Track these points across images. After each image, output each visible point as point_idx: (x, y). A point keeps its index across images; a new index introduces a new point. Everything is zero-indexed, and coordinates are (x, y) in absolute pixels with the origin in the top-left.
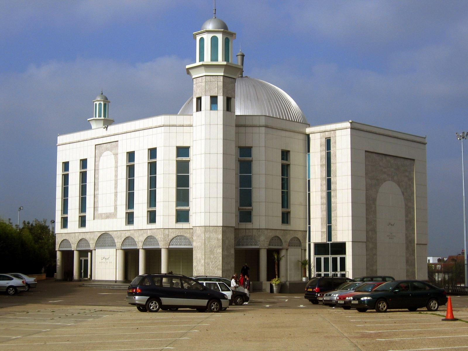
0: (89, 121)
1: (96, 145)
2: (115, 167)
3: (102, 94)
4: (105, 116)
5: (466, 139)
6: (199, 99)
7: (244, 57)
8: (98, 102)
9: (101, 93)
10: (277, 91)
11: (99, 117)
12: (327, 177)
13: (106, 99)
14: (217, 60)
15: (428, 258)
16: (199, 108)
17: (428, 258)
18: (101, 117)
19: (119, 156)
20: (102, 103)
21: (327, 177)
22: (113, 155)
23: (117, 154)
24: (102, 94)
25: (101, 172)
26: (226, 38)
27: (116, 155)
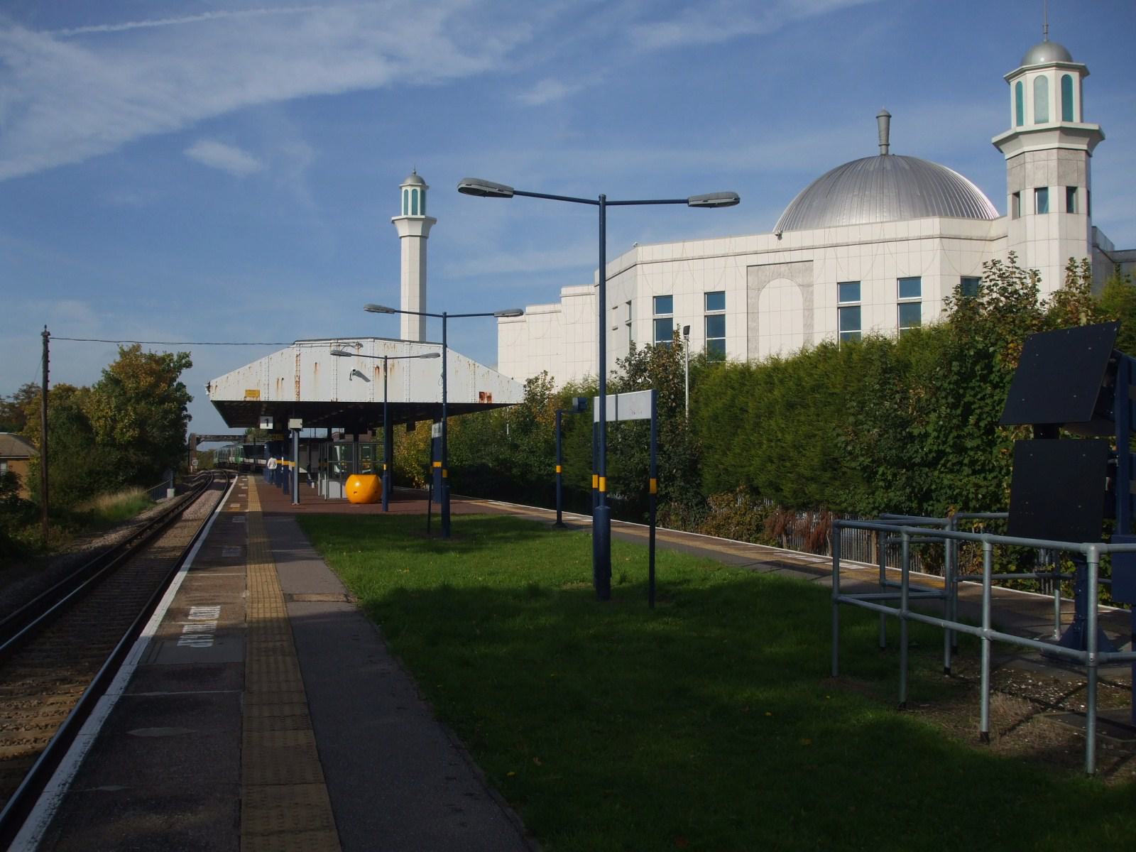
0: (393, 221)
1: (748, 266)
2: (804, 309)
3: (415, 173)
4: (422, 213)
5: (1129, 276)
6: (1042, 192)
7: (891, 119)
8: (408, 188)
9: (414, 172)
10: (964, 184)
11: (413, 214)
12: (841, 330)
13: (423, 182)
14: (1071, 120)
15: (272, 418)
16: (1042, 206)
17: (272, 418)
18: (417, 214)
19: (817, 289)
20: (418, 189)
21: (841, 330)
22: (798, 288)
23: (811, 285)
24: (415, 173)
25: (763, 320)
26: (1063, 77)
27: (807, 287)
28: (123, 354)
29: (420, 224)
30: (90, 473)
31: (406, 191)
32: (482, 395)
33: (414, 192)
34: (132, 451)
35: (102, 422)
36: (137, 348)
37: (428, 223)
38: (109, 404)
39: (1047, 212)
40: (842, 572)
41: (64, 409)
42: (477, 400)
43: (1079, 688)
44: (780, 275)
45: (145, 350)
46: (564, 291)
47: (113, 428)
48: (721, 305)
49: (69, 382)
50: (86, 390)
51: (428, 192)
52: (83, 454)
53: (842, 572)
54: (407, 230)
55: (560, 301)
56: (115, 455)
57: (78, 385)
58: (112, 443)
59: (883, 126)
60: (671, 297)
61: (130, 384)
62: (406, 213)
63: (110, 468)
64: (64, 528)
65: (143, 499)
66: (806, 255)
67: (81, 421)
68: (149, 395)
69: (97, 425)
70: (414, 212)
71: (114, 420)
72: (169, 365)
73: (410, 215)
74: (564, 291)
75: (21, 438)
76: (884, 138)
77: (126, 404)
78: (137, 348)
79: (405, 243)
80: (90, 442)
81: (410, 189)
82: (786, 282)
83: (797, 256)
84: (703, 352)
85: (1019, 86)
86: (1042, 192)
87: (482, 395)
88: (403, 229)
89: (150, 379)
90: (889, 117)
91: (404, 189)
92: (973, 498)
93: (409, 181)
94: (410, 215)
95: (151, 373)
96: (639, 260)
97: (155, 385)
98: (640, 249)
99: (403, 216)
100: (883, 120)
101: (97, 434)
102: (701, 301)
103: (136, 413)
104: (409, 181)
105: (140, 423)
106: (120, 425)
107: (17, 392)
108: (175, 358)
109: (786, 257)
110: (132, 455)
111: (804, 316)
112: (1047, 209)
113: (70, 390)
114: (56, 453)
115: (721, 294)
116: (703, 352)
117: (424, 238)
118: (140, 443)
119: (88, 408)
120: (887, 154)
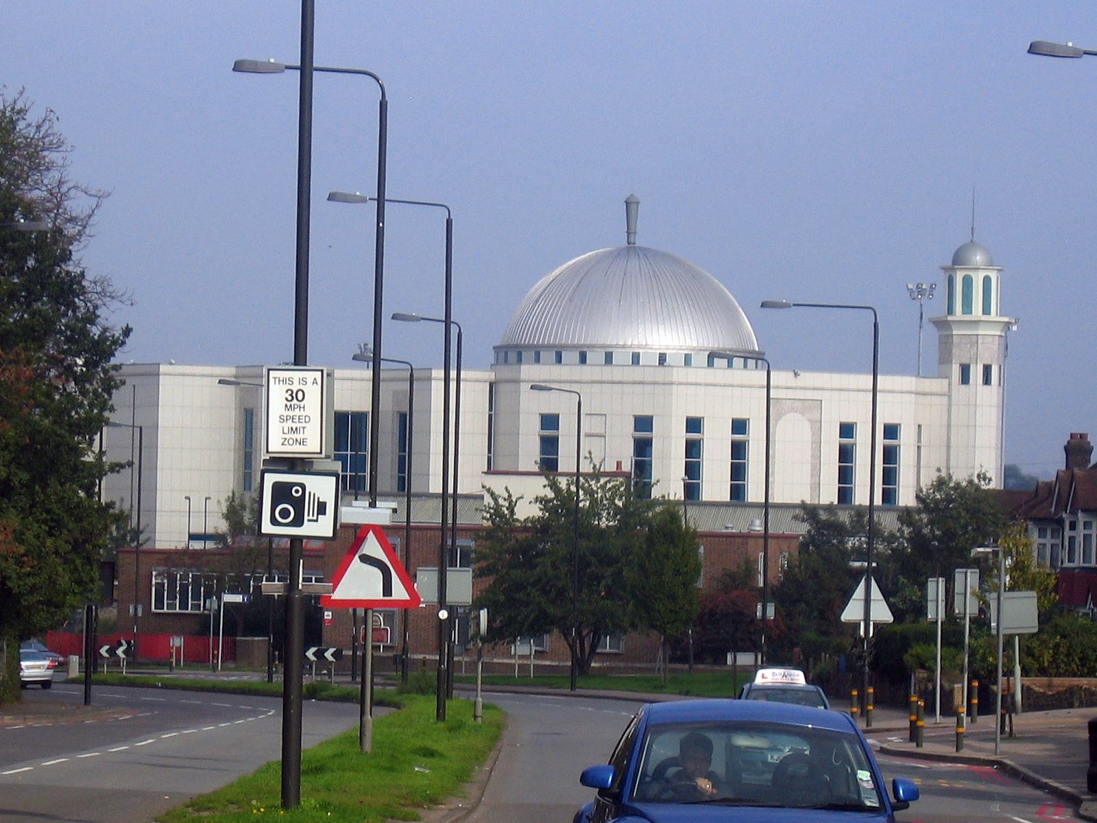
6: (987, 369)
11: (964, 313)
28: (111, 501)
39: (990, 384)
40: (1083, 783)
43: (56, 221)
44: (794, 410)
53: (1083, 783)
60: (733, 421)
66: (816, 395)
82: (798, 416)
83: (809, 395)
84: (71, 267)
86: (987, 369)
92: (1038, 639)
96: (675, 379)
107: (123, 387)
109: (800, 394)
111: (812, 447)
112: (991, 382)
116: (71, 267)
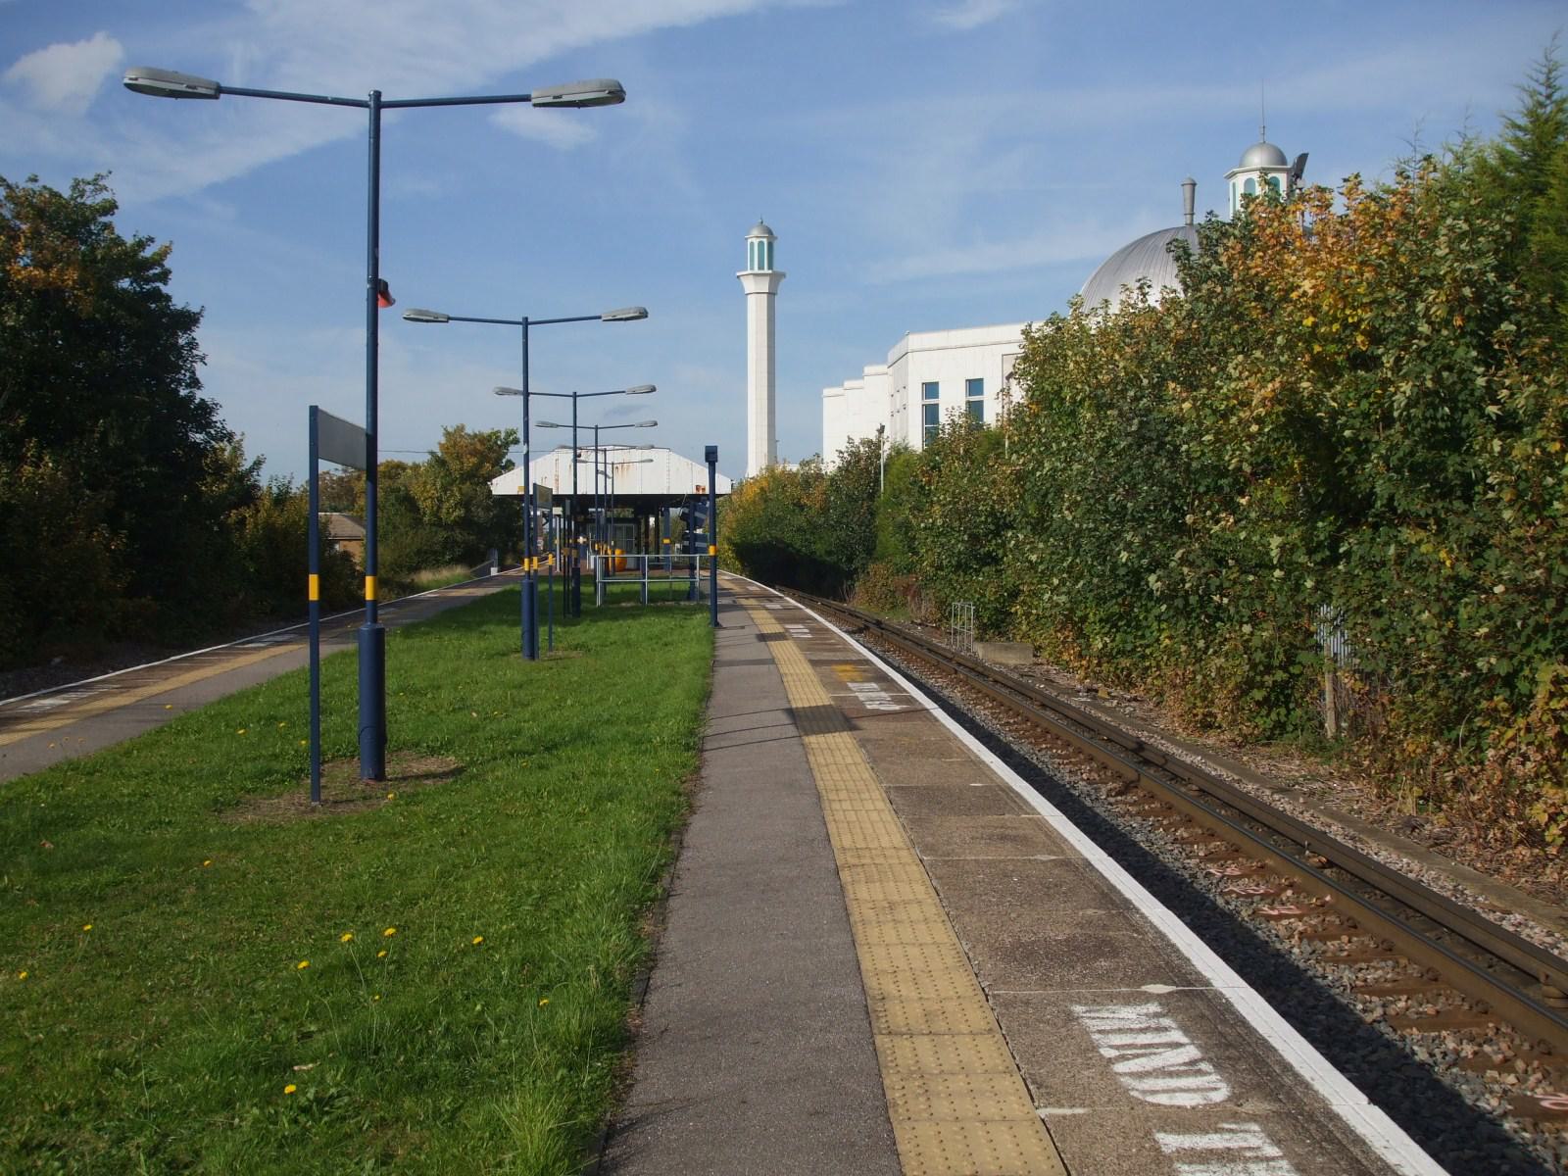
8: (755, 239)
13: (770, 232)
20: (765, 241)
28: (448, 434)
29: (767, 280)
30: (419, 552)
31: (752, 244)
32: (698, 488)
33: (761, 244)
34: (457, 531)
35: (429, 501)
36: (461, 428)
37: (776, 278)
38: (434, 485)
41: (393, 491)
42: (695, 492)
45: (469, 430)
46: (868, 370)
47: (439, 508)
48: (980, 392)
49: (397, 458)
50: (416, 467)
51: (776, 245)
52: (411, 533)
54: (754, 287)
55: (863, 378)
56: (442, 535)
57: (408, 460)
58: (439, 523)
59: (1188, 195)
61: (454, 466)
62: (752, 268)
63: (437, 548)
64: (390, 591)
65: (466, 577)
67: (409, 502)
68: (474, 476)
69: (425, 505)
70: (761, 267)
71: (440, 500)
72: (496, 443)
73: (756, 270)
74: (868, 370)
75: (351, 518)
76: (1188, 207)
77: (452, 485)
78: (461, 428)
79: (751, 300)
80: (418, 522)
81: (756, 241)
85: (1234, 184)
87: (698, 488)
88: (749, 285)
89: (474, 460)
90: (1194, 185)
91: (749, 241)
93: (755, 232)
94: (756, 270)
95: (474, 453)
97: (479, 466)
98: (910, 337)
99: (749, 272)
100: (1188, 188)
101: (425, 514)
102: (962, 387)
103: (462, 494)
104: (755, 232)
105: (465, 504)
106: (446, 505)
108: (503, 435)
110: (459, 535)
113: (401, 467)
114: (386, 534)
115: (970, 382)
117: (771, 294)
118: (465, 523)
119: (415, 490)
120: (1191, 224)
